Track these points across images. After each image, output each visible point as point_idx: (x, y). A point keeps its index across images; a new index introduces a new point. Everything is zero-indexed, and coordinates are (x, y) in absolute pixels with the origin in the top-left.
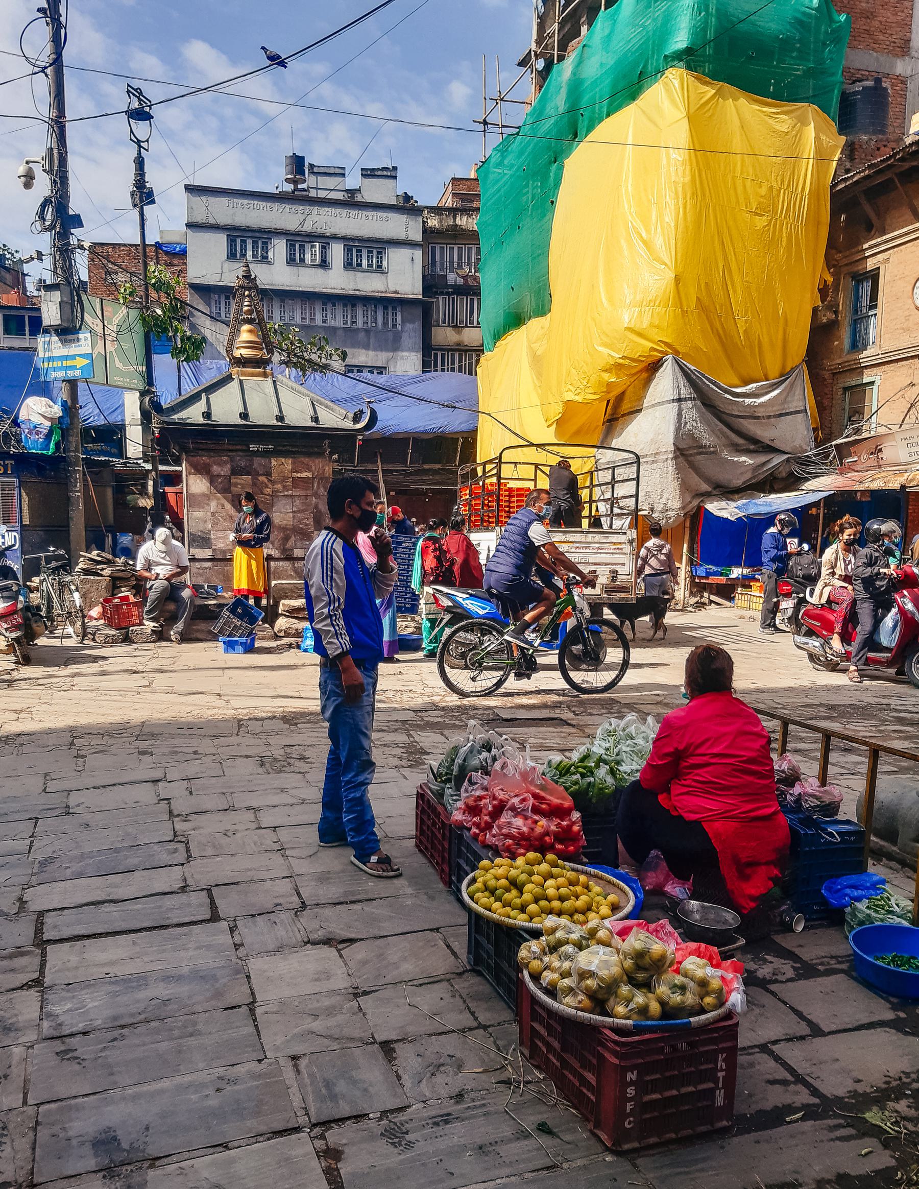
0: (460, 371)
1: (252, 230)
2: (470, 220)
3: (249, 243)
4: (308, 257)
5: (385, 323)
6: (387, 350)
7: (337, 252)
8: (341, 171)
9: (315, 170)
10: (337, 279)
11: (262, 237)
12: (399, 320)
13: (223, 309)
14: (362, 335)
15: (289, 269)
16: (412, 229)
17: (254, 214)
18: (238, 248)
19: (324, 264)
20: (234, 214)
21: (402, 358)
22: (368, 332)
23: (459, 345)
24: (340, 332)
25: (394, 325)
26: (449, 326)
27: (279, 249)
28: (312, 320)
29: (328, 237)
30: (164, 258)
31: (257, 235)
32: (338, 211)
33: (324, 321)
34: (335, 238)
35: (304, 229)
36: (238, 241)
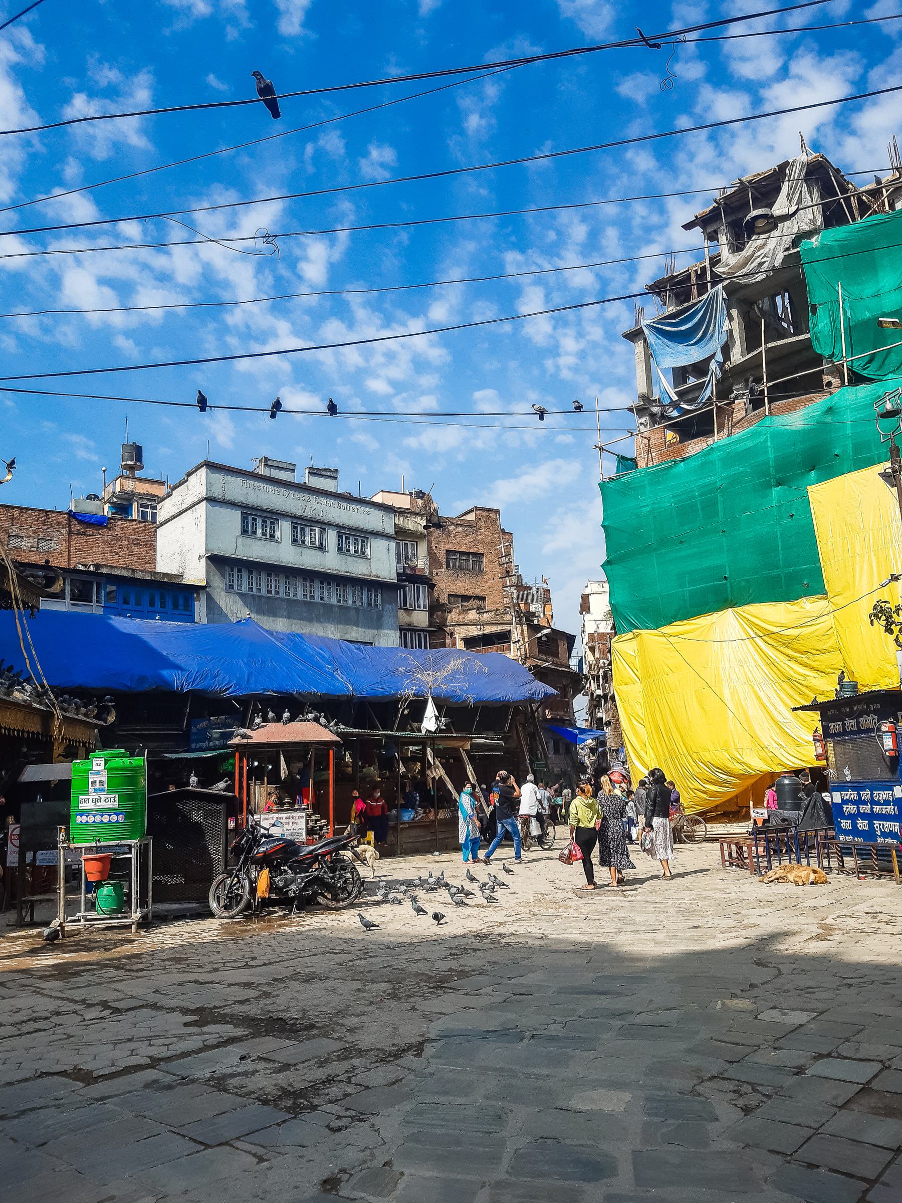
0: (412, 648)
1: (264, 511)
2: (406, 521)
3: (259, 522)
4: (308, 539)
5: (370, 604)
6: (373, 628)
7: (332, 536)
8: (291, 467)
9: (269, 463)
10: (331, 561)
11: (271, 516)
12: (380, 602)
13: (235, 581)
14: (353, 612)
15: (292, 549)
16: (388, 524)
17: (264, 496)
18: (250, 525)
19: (321, 548)
20: (247, 493)
21: (384, 635)
22: (357, 609)
23: (410, 625)
24: (335, 609)
25: (376, 606)
26: (401, 608)
27: (284, 529)
28: (278, 593)
29: (325, 523)
30: (76, 527)
31: (267, 515)
32: (331, 502)
33: (322, 598)
34: (330, 524)
35: (306, 514)
36: (250, 518)
